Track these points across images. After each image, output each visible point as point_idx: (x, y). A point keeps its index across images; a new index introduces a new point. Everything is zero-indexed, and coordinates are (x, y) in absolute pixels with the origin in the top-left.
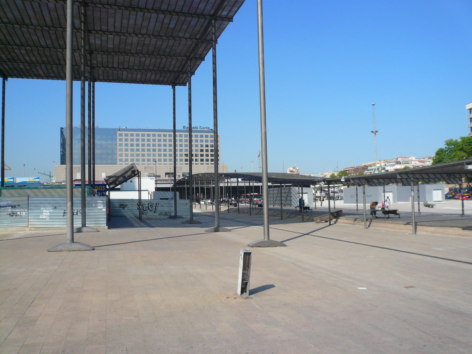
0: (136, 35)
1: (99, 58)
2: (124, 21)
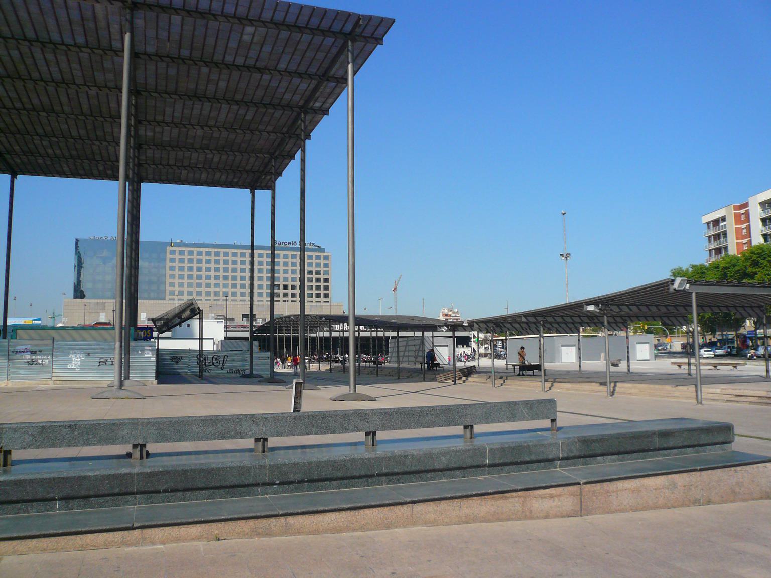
0: (202, 127)
1: (149, 153)
2: (185, 111)
